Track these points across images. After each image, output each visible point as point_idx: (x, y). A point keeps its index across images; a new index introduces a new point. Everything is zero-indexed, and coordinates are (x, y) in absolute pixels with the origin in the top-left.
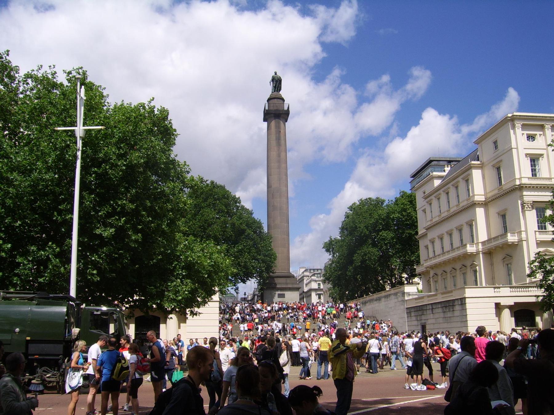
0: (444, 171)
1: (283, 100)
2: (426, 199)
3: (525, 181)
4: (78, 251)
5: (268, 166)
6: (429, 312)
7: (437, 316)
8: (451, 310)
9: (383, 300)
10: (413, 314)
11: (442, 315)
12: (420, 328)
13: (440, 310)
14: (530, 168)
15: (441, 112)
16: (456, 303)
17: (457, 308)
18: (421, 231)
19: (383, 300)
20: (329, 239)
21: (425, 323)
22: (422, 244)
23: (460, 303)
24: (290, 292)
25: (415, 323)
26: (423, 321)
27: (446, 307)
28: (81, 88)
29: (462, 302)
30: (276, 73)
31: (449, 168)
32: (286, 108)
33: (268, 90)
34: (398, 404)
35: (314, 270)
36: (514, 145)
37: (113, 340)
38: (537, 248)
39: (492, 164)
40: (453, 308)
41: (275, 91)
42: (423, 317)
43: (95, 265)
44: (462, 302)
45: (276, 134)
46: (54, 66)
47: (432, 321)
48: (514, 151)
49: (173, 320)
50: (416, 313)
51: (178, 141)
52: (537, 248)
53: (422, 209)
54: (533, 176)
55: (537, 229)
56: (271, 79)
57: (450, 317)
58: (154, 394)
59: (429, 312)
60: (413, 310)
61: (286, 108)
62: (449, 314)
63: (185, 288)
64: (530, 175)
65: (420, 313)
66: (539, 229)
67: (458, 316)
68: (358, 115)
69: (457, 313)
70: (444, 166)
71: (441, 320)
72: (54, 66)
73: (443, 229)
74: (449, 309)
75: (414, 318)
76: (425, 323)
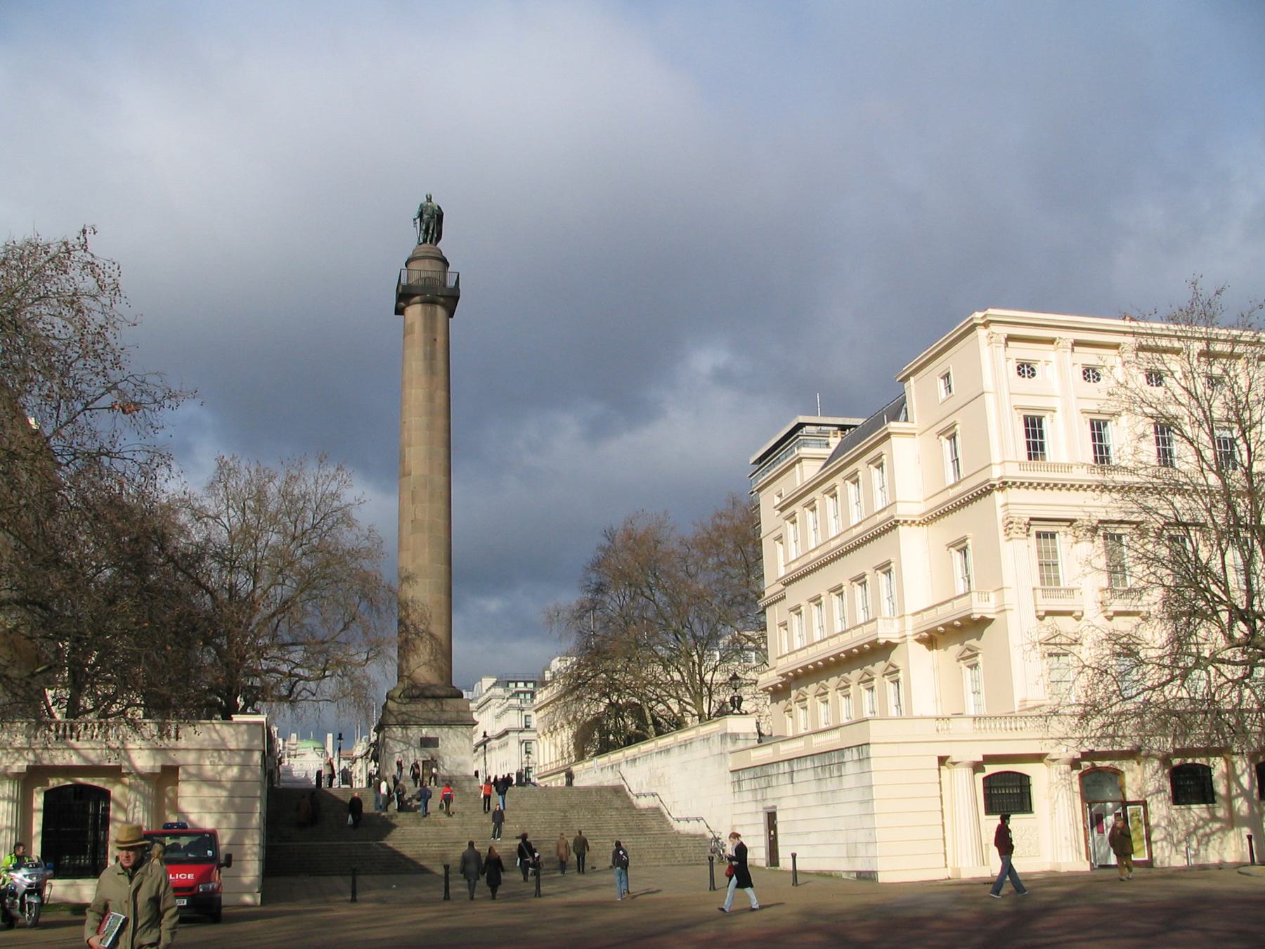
0: (828, 444)
1: (447, 264)
2: (782, 510)
3: (1013, 472)
9: (676, 751)
10: (746, 785)
11: (813, 786)
12: (762, 818)
13: (810, 775)
14: (1045, 439)
15: (1054, 879)
16: (848, 755)
17: (850, 768)
18: (770, 587)
19: (676, 751)
20: (1189, 295)
21: (775, 807)
22: (774, 616)
23: (856, 757)
24: (1064, 869)
25: (752, 807)
26: (770, 804)
30: (429, 199)
31: (839, 440)
32: (451, 283)
33: (410, 236)
34: (913, 393)
36: (988, 383)
37: (684, 598)
40: (839, 770)
41: (425, 241)
42: (770, 793)
43: (279, 682)
47: (794, 802)
48: (989, 399)
49: (143, 744)
50: (754, 784)
53: (776, 534)
54: (1030, 458)
55: (1037, 583)
56: (416, 210)
57: (833, 791)
58: (1000, 863)
61: (451, 283)
62: (831, 784)
64: (1089, 456)
65: (763, 782)
66: (1043, 583)
67: (851, 789)
68: (989, 616)
69: (849, 782)
70: (827, 434)
71: (811, 800)
73: (819, 583)
75: (749, 796)
76: (775, 807)
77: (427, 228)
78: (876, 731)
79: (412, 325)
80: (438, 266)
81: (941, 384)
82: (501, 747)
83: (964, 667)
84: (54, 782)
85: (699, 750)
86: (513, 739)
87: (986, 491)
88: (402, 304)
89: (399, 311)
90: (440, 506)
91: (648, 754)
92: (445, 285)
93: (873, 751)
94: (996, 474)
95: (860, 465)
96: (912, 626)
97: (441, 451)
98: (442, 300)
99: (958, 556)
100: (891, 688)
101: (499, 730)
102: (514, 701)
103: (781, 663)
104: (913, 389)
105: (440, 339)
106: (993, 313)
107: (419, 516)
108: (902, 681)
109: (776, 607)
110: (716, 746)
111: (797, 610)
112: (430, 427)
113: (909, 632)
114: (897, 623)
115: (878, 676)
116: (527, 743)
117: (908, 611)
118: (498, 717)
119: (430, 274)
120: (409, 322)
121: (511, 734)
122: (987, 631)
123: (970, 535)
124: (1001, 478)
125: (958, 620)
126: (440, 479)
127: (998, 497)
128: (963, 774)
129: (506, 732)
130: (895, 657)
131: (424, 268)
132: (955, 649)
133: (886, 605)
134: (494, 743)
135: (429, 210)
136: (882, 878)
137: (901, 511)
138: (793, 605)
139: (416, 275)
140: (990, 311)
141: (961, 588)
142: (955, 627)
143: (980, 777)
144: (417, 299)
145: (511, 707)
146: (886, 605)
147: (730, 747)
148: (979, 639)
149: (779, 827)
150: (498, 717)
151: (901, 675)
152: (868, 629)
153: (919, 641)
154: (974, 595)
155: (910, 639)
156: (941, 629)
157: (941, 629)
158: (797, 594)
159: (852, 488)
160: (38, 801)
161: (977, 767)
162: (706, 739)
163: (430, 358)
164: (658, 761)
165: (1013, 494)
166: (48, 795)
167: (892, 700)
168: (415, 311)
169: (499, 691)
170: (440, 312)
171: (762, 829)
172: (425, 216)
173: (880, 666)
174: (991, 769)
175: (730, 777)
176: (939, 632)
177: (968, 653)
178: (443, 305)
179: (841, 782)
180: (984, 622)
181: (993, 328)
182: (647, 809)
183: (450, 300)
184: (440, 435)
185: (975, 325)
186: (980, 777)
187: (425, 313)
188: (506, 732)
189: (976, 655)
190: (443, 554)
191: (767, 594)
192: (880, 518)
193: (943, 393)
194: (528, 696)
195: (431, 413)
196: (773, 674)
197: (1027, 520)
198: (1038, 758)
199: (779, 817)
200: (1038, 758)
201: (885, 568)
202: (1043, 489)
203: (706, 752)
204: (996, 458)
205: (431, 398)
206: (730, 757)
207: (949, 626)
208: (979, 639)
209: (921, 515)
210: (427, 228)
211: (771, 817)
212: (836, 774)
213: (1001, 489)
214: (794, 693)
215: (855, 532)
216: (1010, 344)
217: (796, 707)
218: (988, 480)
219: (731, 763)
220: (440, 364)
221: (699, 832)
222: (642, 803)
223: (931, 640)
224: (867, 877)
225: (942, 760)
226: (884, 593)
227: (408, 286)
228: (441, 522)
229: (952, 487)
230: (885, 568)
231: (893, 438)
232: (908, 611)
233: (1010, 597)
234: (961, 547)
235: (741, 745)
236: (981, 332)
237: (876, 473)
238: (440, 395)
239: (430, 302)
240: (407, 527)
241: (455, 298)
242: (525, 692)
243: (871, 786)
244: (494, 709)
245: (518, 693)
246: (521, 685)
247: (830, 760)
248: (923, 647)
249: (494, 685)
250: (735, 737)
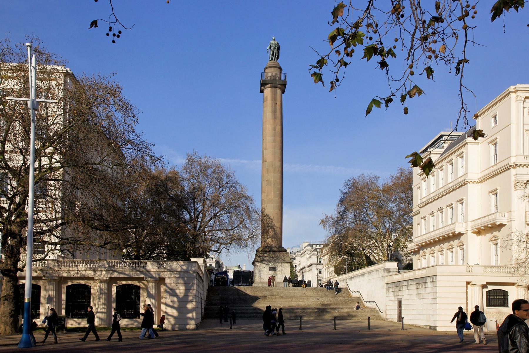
4: (28, 187)
5: (282, 199)
6: (405, 288)
7: (411, 292)
8: (424, 287)
9: (366, 275)
10: (391, 290)
11: (415, 291)
12: (396, 303)
13: (414, 287)
17: (429, 285)
18: (415, 209)
19: (366, 275)
22: (416, 220)
23: (431, 281)
25: (393, 298)
26: (399, 297)
27: (419, 284)
28: (31, 56)
29: (433, 279)
32: (283, 78)
34: (480, 124)
35: (316, 245)
36: (514, 120)
38: (508, 306)
39: (151, 304)
40: (425, 285)
41: (272, 59)
42: (400, 293)
44: (433, 279)
45: (272, 105)
46: (346, 64)
48: (513, 128)
50: (394, 289)
51: (519, 298)
52: (508, 306)
53: (418, 186)
59: (405, 288)
60: (391, 286)
61: (283, 78)
62: (422, 291)
63: (38, 193)
65: (397, 289)
67: (429, 293)
69: (428, 290)
72: (346, 64)
73: (433, 207)
74: (422, 286)
75: (392, 294)
77: (273, 53)
78: (439, 270)
79: (267, 97)
80: (277, 70)
81: (493, 120)
82: (309, 271)
83: (492, 244)
84: (70, 283)
85: (375, 275)
86: (314, 268)
87: (508, 168)
88: (263, 88)
89: (262, 91)
90: (278, 174)
91: (356, 276)
92: (280, 79)
93: (438, 278)
94: (513, 161)
95: (454, 157)
96: (470, 226)
97: (279, 151)
98: (279, 86)
99: (493, 197)
100: (460, 252)
101: (309, 264)
102: (315, 252)
103: (416, 240)
104: (480, 122)
105: (278, 103)
106: (520, 86)
107: (270, 179)
108: (465, 249)
109: (416, 216)
110: (381, 274)
111: (424, 218)
112: (274, 141)
113: (469, 229)
114: (464, 225)
115: (455, 247)
116: (320, 269)
117: (470, 219)
118: (308, 259)
119: (274, 75)
120: (265, 96)
121: (313, 266)
122: (503, 229)
123: (498, 188)
124: (515, 163)
125: (490, 224)
126: (278, 163)
127: (513, 171)
128: (478, 289)
129: (311, 265)
130: (462, 238)
131: (271, 72)
132: (489, 236)
133: (460, 217)
134: (307, 269)
135: (274, 45)
136: (439, 329)
137: (469, 177)
138: (423, 216)
139: (268, 75)
140: (518, 85)
141: (493, 210)
142: (489, 227)
143: (485, 290)
144: (269, 85)
145: (313, 254)
146: (460, 217)
147: (386, 274)
148: (499, 232)
149: (402, 306)
150: (308, 259)
151: (464, 247)
152: (452, 227)
153: (474, 232)
154: (498, 214)
155: (469, 232)
156: (483, 228)
157: (483, 228)
158: (425, 211)
159: (450, 166)
160: (64, 290)
161: (484, 287)
162: (378, 270)
163: (274, 111)
164: (360, 279)
165: (520, 170)
166: (68, 287)
167: (460, 257)
168: (268, 91)
169: (309, 248)
170: (279, 91)
171: (396, 307)
172: (272, 48)
173: (456, 242)
174: (490, 288)
175: (385, 286)
176: (482, 229)
177: (494, 238)
178: (279, 88)
179: (425, 290)
180: (501, 226)
181: (519, 93)
182: (355, 298)
183: (283, 86)
184: (278, 144)
185: (510, 92)
186: (485, 290)
187: (272, 92)
188: (311, 265)
189: (497, 239)
190: (279, 193)
191: (414, 210)
192: (460, 180)
193: (493, 124)
194: (320, 250)
195: (274, 135)
196: (413, 244)
197: (525, 182)
198: (513, 284)
199: (403, 303)
200: (513, 284)
201: (461, 201)
202: (519, 167)
203: (377, 276)
204: (514, 153)
205: (274, 129)
206: (386, 278)
207: (486, 227)
208: (499, 232)
209: (478, 179)
210: (273, 53)
211: (400, 302)
212: (424, 287)
213: (515, 167)
214: (421, 251)
215: (450, 185)
216: (526, 100)
217: (422, 258)
218: (509, 164)
219: (387, 280)
220: (278, 114)
221: (374, 307)
222: (354, 295)
223: (479, 232)
224: (434, 328)
225: (468, 283)
226: (460, 212)
227: (265, 80)
228: (279, 181)
229: (493, 166)
230: (461, 201)
231: (469, 145)
232: (470, 219)
233: (514, 214)
234: (495, 193)
235: (391, 273)
236: (513, 96)
237: (460, 160)
238: (278, 128)
239: (274, 87)
240: (265, 183)
241: (285, 85)
242: (319, 249)
243: (436, 293)
244: (306, 256)
245: (316, 249)
246: (318, 246)
247: (421, 282)
248: (475, 235)
249: (307, 246)
250: (389, 271)
